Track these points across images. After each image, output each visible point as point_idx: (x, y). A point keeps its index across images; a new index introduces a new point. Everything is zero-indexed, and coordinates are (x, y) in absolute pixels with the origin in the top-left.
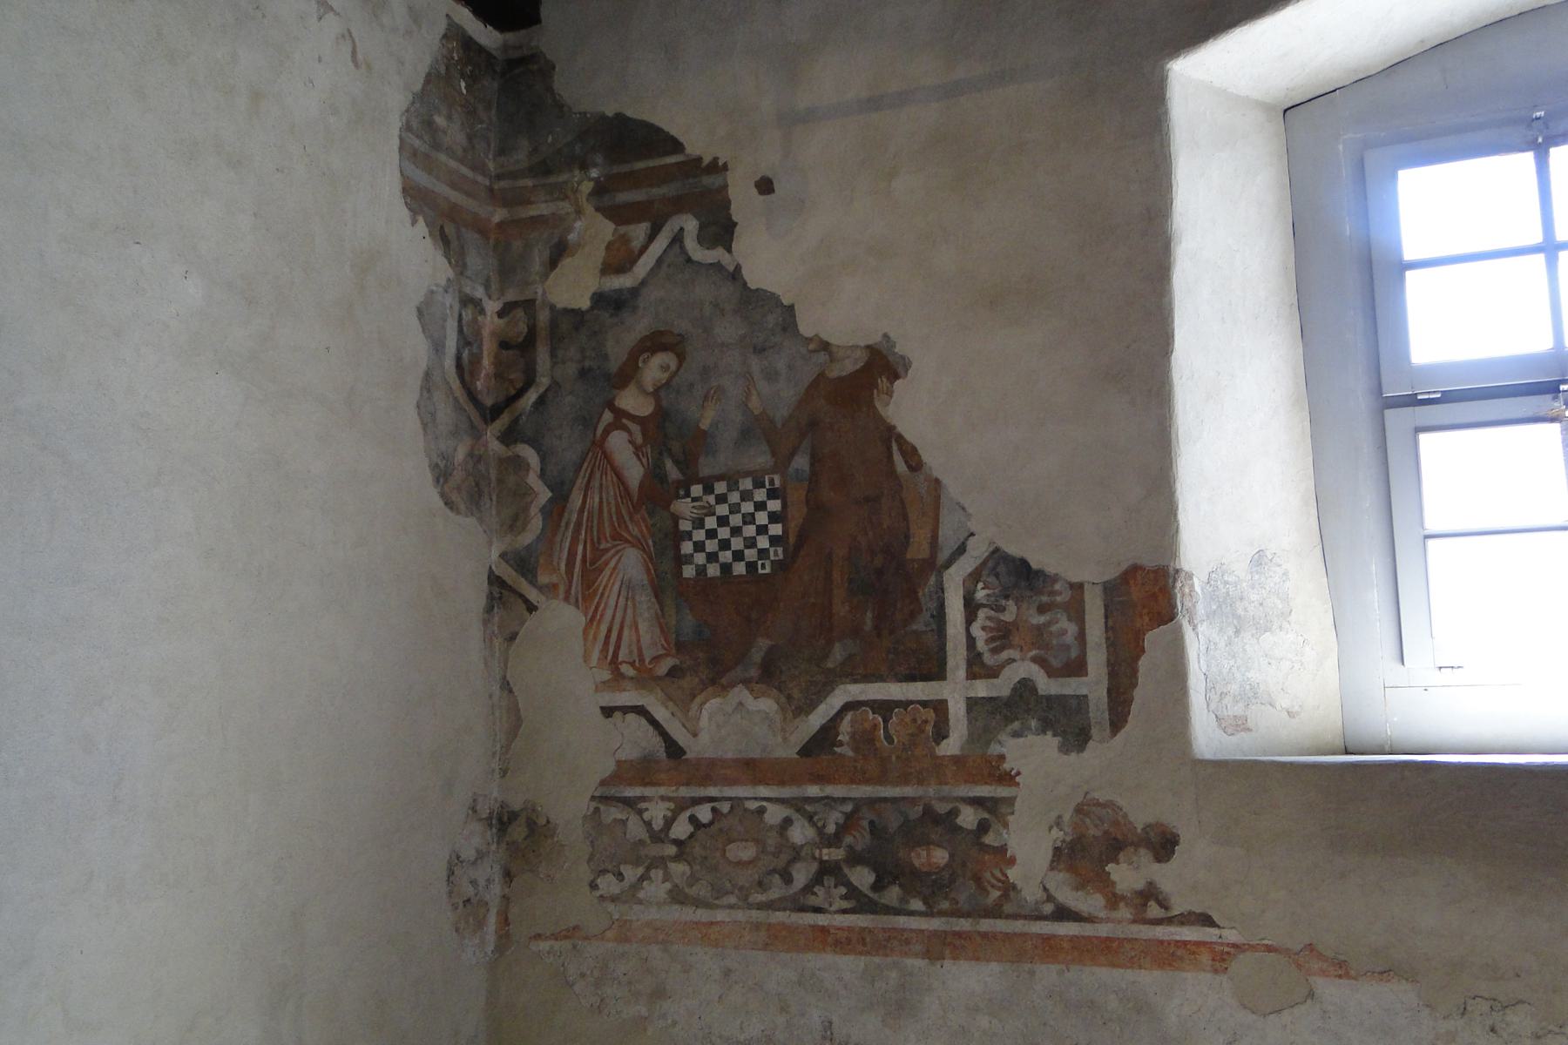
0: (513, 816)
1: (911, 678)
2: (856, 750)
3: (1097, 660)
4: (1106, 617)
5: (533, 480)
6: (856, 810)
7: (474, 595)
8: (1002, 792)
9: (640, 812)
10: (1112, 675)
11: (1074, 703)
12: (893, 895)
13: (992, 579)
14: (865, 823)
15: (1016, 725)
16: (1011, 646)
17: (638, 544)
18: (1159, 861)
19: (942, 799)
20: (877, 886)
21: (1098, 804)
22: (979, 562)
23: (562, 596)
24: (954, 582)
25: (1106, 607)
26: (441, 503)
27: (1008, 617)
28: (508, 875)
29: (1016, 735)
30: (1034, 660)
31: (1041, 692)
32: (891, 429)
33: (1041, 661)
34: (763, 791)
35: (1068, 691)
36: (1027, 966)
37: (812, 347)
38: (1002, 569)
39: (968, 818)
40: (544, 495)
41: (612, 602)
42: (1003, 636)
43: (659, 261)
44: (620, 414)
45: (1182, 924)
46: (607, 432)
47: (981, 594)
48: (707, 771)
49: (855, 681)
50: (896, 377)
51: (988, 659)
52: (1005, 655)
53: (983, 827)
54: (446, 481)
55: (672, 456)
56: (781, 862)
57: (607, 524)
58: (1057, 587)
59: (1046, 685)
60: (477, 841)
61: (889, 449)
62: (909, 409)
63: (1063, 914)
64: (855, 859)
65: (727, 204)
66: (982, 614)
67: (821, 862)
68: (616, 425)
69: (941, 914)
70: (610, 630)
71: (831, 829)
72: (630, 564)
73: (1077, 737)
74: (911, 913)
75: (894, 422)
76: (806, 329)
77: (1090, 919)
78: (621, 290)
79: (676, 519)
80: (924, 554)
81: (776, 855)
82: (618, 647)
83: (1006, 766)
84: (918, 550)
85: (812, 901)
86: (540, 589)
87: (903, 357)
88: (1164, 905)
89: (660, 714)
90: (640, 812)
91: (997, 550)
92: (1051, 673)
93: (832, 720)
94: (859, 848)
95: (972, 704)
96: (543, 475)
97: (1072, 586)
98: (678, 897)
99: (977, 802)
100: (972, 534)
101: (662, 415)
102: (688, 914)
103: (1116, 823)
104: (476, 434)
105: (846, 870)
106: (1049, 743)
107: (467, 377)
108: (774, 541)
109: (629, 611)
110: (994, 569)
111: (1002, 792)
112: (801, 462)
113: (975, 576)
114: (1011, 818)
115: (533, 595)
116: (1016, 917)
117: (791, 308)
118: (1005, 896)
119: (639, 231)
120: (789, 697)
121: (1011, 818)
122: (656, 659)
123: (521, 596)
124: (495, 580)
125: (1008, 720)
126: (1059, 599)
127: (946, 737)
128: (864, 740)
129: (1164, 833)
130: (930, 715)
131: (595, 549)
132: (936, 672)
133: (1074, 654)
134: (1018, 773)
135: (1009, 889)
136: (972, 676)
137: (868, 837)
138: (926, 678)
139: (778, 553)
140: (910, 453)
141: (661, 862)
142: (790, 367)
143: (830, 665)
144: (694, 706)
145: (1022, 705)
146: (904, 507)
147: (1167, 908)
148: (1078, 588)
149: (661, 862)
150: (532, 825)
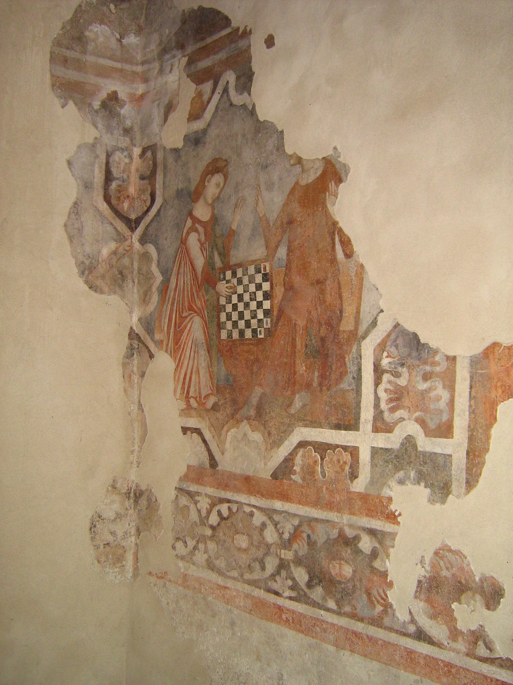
0: (141, 493)
1: (338, 427)
2: (304, 479)
3: (461, 423)
4: (471, 388)
5: (154, 269)
6: (300, 525)
7: (118, 347)
8: (388, 527)
9: (196, 503)
10: (471, 439)
11: (441, 460)
12: (317, 593)
13: (393, 349)
14: (305, 535)
15: (401, 474)
16: (403, 407)
17: (200, 314)
18: (488, 608)
19: (351, 526)
20: (309, 585)
21: (450, 550)
22: (385, 334)
23: (164, 348)
24: (368, 349)
25: (472, 378)
26: (86, 288)
27: (402, 382)
28: (139, 531)
29: (401, 482)
30: (417, 420)
31: (420, 449)
32: (335, 223)
33: (422, 422)
34: (253, 500)
35: (438, 450)
36: (394, 670)
37: (292, 162)
38: (400, 341)
39: (366, 544)
40: (159, 278)
41: (188, 355)
42: (398, 397)
43: (217, 108)
44: (196, 220)
45: (501, 666)
46: (188, 233)
47: (385, 362)
48: (226, 482)
49: (306, 426)
50: (340, 180)
51: (387, 416)
52: (399, 414)
53: (374, 554)
54: (91, 273)
55: (217, 249)
56: (260, 554)
57: (186, 299)
58: (437, 358)
59: (425, 444)
60: (116, 506)
61: (333, 240)
62: (348, 208)
63: (421, 635)
64: (298, 562)
65: (250, 59)
66: (386, 377)
67: (281, 559)
68: (193, 229)
69: (346, 615)
70: (185, 375)
71: (286, 536)
72: (196, 328)
73: (442, 490)
74: (328, 610)
75: (337, 219)
76: (289, 150)
77: (439, 645)
78: (196, 132)
79: (218, 295)
80: (351, 327)
81: (258, 548)
82: (189, 387)
83: (393, 507)
84: (347, 325)
85: (275, 586)
86: (155, 342)
87: (345, 165)
88: (489, 647)
89: (208, 436)
90: (196, 503)
91: (397, 326)
92: (429, 433)
93: (291, 454)
94: (301, 553)
95: (375, 451)
96: (159, 265)
97: (448, 358)
98: (210, 566)
99: (372, 532)
100: (382, 311)
101: (215, 219)
102: (214, 577)
103: (462, 569)
104: (121, 238)
105: (293, 568)
106: (422, 492)
107: (114, 201)
108: (267, 313)
109: (196, 361)
110: (395, 341)
111: (388, 527)
112: (282, 252)
113: (382, 347)
114: (391, 550)
115: (152, 347)
116: (391, 629)
117: (282, 132)
118: (385, 611)
119: (207, 87)
120: (269, 434)
121: (391, 550)
122: (207, 396)
123: (147, 347)
124: (133, 335)
125: (397, 469)
126: (438, 369)
127: (356, 477)
128: (309, 472)
129: (493, 584)
130: (347, 457)
131: (181, 317)
132: (350, 424)
133: (445, 417)
134: (400, 515)
135: (387, 606)
136: (376, 430)
137: (306, 547)
138: (347, 428)
139: (267, 323)
140: (346, 243)
141: (202, 539)
142: (280, 179)
143: (293, 411)
144: (224, 432)
145: (403, 459)
146: (340, 288)
147: (491, 650)
148: (453, 359)
149: (202, 539)
150: (149, 500)
